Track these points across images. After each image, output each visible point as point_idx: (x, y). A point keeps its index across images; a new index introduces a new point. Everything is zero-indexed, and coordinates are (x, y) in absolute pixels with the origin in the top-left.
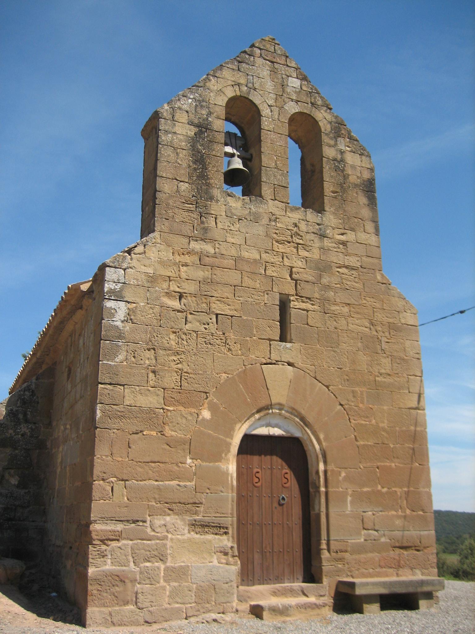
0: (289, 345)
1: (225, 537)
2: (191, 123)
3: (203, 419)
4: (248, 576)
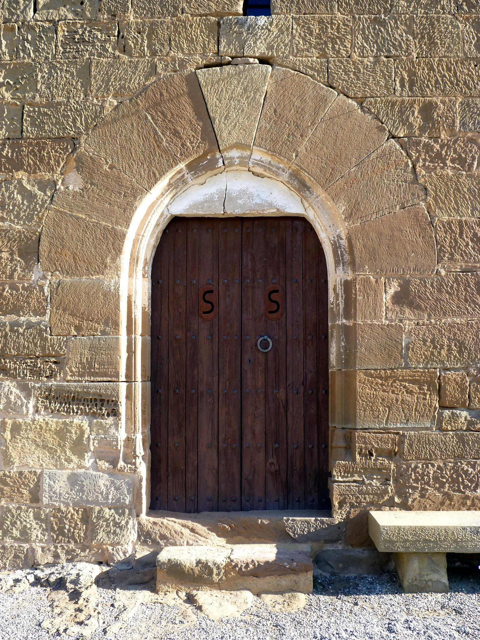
0: (262, 20)
1: (110, 420)
3: (66, 193)
4: (174, 488)
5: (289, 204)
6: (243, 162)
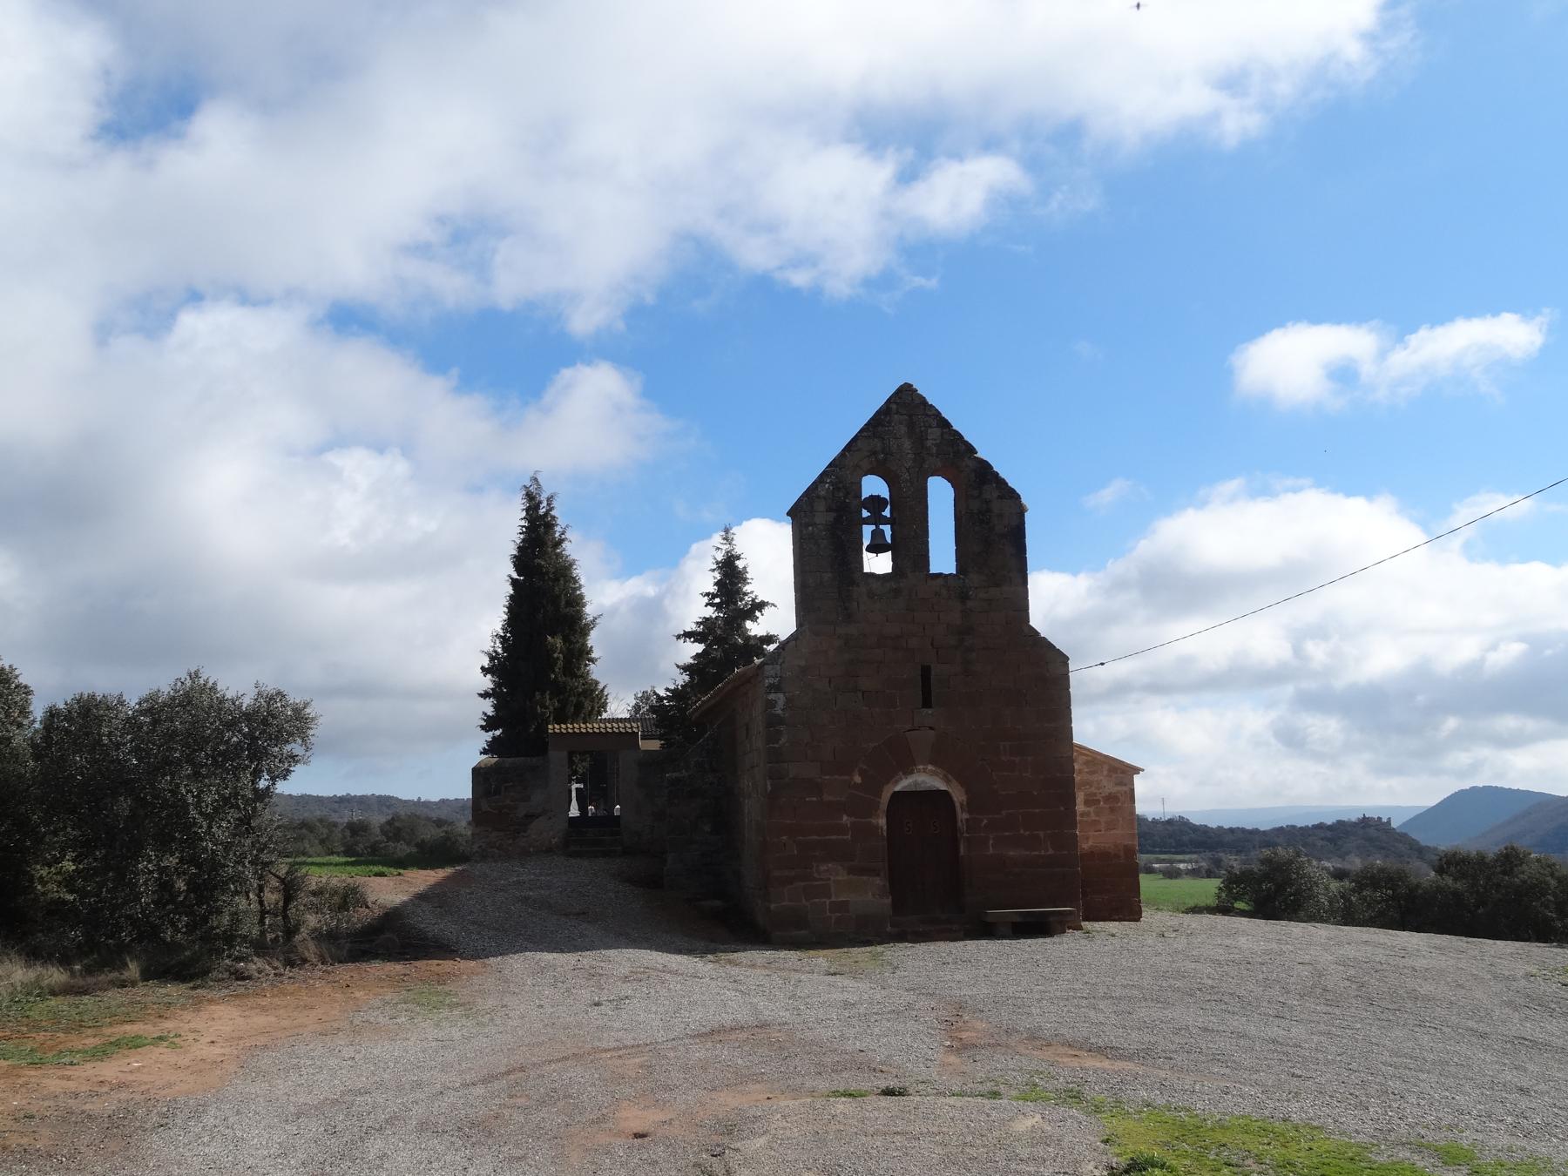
2: (829, 510)
5: (943, 787)
6: (925, 771)
